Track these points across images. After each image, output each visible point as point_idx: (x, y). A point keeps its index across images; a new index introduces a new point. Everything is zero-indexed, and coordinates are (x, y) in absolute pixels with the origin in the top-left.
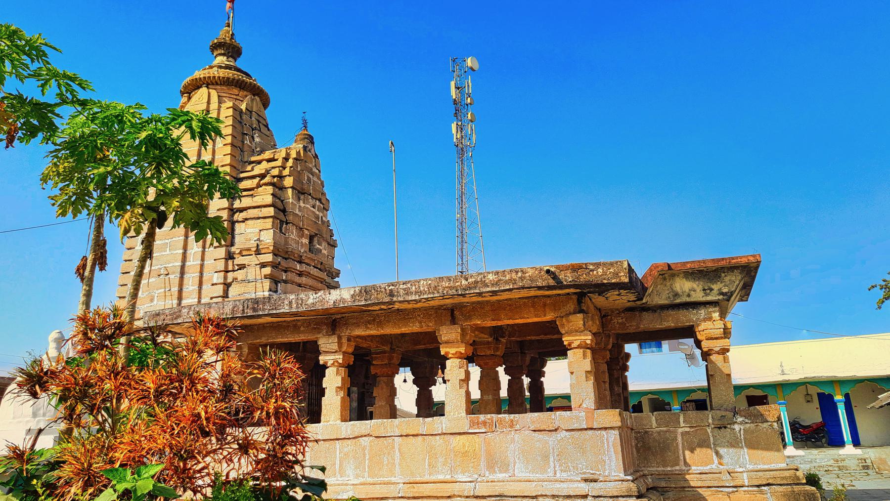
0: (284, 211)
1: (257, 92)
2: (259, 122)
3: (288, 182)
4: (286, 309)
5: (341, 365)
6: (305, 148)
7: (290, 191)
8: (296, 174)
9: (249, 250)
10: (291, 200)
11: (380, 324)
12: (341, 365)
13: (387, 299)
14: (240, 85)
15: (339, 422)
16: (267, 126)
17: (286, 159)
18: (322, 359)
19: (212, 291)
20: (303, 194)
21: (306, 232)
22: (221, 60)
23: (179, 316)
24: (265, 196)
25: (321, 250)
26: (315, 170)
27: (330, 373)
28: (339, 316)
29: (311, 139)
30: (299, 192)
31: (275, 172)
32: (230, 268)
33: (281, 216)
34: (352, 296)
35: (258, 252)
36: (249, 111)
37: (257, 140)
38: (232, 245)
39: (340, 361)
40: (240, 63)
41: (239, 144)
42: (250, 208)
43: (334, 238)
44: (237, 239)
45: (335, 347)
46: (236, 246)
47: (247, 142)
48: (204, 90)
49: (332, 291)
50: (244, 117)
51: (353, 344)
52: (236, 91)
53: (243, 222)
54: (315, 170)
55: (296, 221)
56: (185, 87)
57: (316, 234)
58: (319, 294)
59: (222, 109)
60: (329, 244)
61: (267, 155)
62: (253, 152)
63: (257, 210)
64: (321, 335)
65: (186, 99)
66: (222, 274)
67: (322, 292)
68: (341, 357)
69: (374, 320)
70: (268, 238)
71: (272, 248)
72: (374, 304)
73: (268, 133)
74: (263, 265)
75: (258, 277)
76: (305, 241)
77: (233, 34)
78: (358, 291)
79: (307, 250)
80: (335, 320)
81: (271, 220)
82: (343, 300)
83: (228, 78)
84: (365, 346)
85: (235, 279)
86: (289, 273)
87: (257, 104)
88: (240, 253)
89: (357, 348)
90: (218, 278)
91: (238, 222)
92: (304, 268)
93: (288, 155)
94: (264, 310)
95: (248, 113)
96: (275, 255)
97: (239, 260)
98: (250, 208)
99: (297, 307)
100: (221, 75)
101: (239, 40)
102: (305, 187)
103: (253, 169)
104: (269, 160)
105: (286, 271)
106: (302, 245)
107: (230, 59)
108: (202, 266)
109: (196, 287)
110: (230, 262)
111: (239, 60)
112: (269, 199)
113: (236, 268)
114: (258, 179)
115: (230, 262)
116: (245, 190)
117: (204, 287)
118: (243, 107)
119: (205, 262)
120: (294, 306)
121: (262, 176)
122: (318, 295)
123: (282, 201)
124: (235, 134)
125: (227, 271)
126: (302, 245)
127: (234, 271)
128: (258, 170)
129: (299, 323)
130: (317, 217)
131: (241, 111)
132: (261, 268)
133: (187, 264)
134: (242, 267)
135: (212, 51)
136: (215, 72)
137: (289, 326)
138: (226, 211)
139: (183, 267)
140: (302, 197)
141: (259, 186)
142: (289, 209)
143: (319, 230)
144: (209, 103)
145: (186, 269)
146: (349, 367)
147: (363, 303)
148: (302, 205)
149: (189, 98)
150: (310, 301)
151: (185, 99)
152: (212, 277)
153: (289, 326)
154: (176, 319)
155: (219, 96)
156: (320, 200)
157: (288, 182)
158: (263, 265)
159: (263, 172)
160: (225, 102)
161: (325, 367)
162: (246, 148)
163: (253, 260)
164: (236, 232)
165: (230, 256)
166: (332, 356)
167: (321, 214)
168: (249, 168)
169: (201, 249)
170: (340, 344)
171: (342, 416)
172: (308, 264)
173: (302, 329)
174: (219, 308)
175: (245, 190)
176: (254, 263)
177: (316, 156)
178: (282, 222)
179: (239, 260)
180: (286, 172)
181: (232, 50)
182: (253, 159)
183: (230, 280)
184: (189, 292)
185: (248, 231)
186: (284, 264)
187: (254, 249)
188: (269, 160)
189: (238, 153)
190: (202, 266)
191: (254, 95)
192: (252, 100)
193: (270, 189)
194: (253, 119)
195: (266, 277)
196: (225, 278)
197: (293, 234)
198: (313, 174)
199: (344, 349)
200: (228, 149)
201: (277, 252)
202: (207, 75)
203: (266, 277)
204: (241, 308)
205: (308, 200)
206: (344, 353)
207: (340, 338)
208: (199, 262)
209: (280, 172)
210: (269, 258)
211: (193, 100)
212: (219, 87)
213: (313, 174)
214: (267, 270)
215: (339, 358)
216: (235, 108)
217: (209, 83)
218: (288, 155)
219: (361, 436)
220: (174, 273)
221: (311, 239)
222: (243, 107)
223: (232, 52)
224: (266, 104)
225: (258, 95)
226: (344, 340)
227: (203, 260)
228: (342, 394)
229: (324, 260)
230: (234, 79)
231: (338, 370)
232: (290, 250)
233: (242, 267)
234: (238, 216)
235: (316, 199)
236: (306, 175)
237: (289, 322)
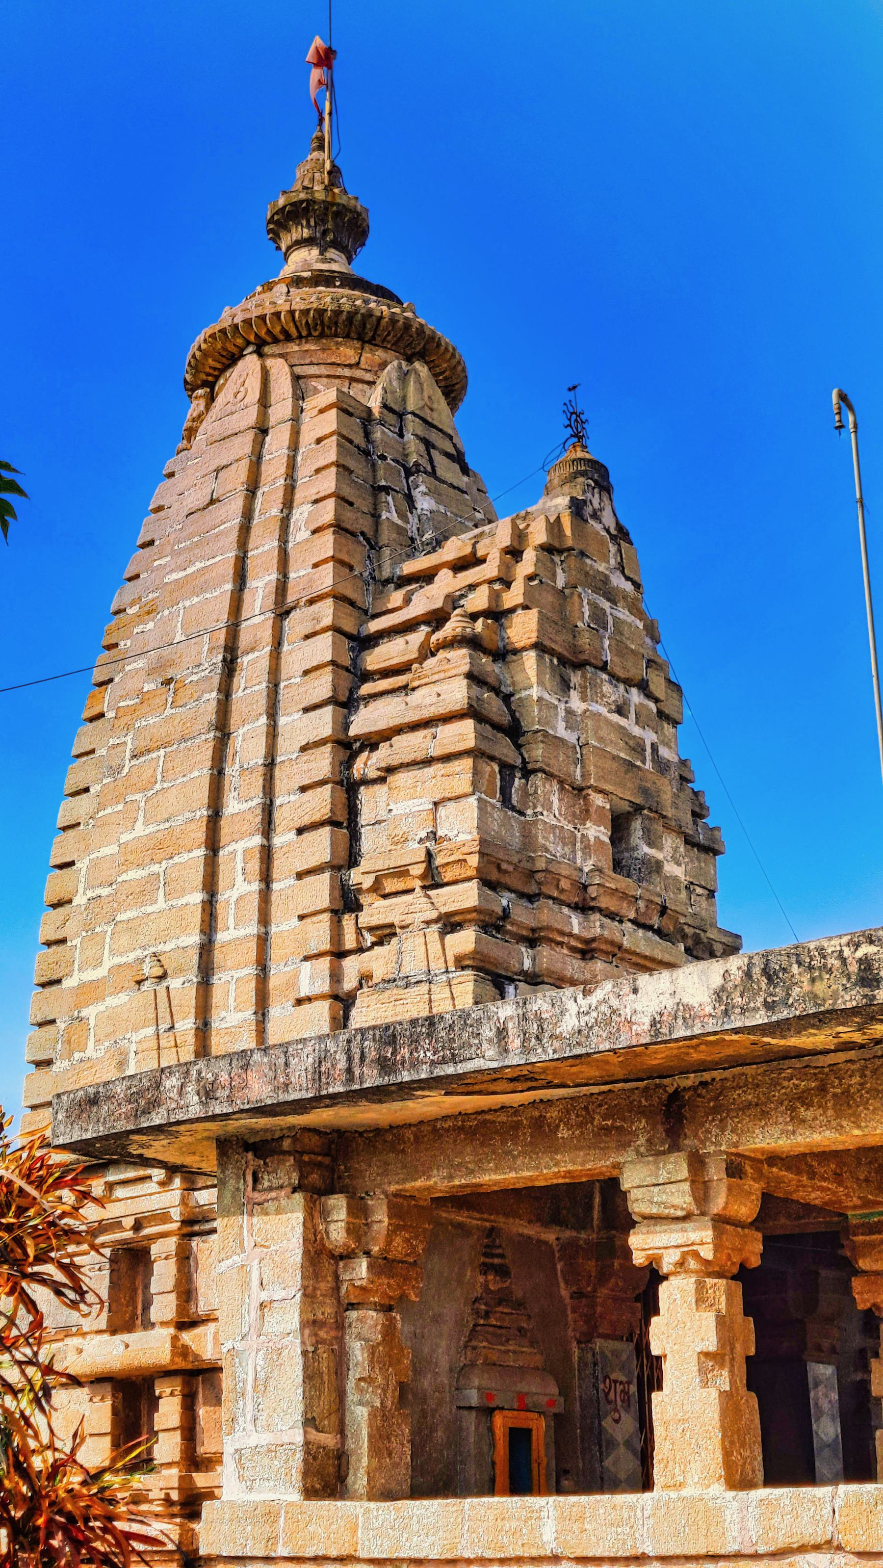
0: (514, 731)
1: (414, 345)
2: (428, 445)
3: (523, 629)
4: (487, 1059)
5: (710, 1269)
6: (577, 507)
7: (530, 659)
8: (549, 598)
9: (401, 872)
10: (535, 692)
11: (846, 1104)
12: (710, 1269)
13: (851, 999)
14: (361, 330)
15: (718, 1489)
16: (458, 458)
17: (514, 553)
18: (641, 1244)
19: (301, 1023)
20: (579, 666)
21: (598, 800)
22: (305, 259)
23: (155, 1103)
24: (446, 684)
25: (657, 866)
26: (618, 581)
27: (674, 1294)
28: (691, 1080)
29: (599, 476)
30: (563, 661)
31: (479, 600)
32: (350, 942)
33: (505, 749)
34: (719, 994)
35: (432, 880)
36: (396, 413)
37: (424, 504)
38: (353, 859)
39: (707, 1253)
40: (364, 265)
41: (365, 524)
42: (399, 730)
43: (710, 821)
44: (368, 841)
45: (681, 1197)
46: (365, 864)
47: (390, 514)
48: (250, 364)
49: (643, 980)
50: (378, 434)
51: (756, 1187)
52: (348, 352)
53: (382, 780)
54: (618, 581)
55: (559, 763)
56: (196, 366)
57: (638, 809)
58: (599, 994)
59: (306, 417)
60: (690, 842)
61: (453, 549)
62: (411, 548)
63: (421, 734)
64: (629, 1155)
65: (202, 403)
66: (325, 963)
67: (608, 986)
68: (708, 1235)
69: (822, 1089)
70: (461, 826)
71: (474, 861)
72: (803, 1022)
73: (463, 481)
74: (450, 924)
75: (437, 966)
76: (597, 832)
77: (335, 172)
78: (737, 975)
79: (606, 864)
80: (676, 1095)
81: (467, 763)
82: (685, 1012)
83: (321, 312)
84: (815, 1197)
85: (365, 978)
86: (544, 951)
87: (421, 389)
88: (376, 888)
89: (770, 1203)
90: (312, 982)
91: (366, 782)
92: (596, 927)
93: (520, 536)
94: (415, 1064)
95: (391, 418)
96: (488, 884)
97: (375, 912)
98: (399, 730)
99: (525, 1049)
100: (298, 305)
101: (357, 192)
102: (585, 640)
103: (407, 601)
104: (460, 566)
105: (532, 942)
106: (587, 848)
107: (332, 253)
108: (263, 941)
109: (249, 1014)
110: (348, 921)
111: (364, 255)
112: (457, 694)
113: (369, 939)
114: (424, 629)
115: (348, 921)
116: (386, 673)
117: (275, 1012)
118: (374, 402)
119: (274, 929)
120: (515, 1043)
121: (437, 619)
122: (593, 999)
123: (507, 699)
124: (347, 492)
125: (339, 954)
126: (587, 848)
127: (360, 950)
128: (426, 599)
129: (553, 1114)
130: (638, 748)
131: (367, 419)
132: (443, 933)
133: (221, 937)
134: (385, 934)
135: (276, 239)
136: (280, 299)
137: (516, 1126)
138: (328, 748)
139: (206, 949)
140: (576, 678)
141: (427, 652)
142: (532, 719)
143: (645, 791)
144: (264, 402)
145: (218, 956)
146: (743, 1275)
147: (760, 1018)
148: (577, 704)
149: (211, 399)
150: (569, 1024)
151: (197, 406)
152: (296, 975)
153: (517, 1126)
154: (146, 1112)
155: (297, 379)
156: (643, 686)
157: (523, 629)
158: (450, 924)
159: (439, 604)
160: (316, 391)
161: (654, 1276)
162: (386, 535)
163: (415, 908)
164: (363, 819)
165: (347, 902)
166: (677, 1227)
167: (649, 737)
168: (396, 597)
169: (256, 886)
170: (701, 1190)
171: (728, 1464)
172: (612, 916)
173: (563, 1133)
174: (274, 1067)
175: (386, 673)
176: (419, 918)
177: (621, 535)
178: (507, 769)
179: (375, 912)
180: (514, 596)
181: (341, 227)
182: (409, 567)
183: (349, 983)
184: (228, 1031)
185: (399, 809)
186: (524, 916)
187: (418, 870)
188: (460, 566)
189: (357, 554)
190: (263, 941)
191: (409, 360)
192: (404, 377)
193: (460, 659)
194: (409, 437)
195: (461, 963)
196: (336, 976)
197: (551, 808)
198: (612, 596)
199: (718, 1203)
200: (326, 544)
201: (494, 876)
202: (255, 313)
203: (461, 963)
204: (342, 1064)
205: (595, 685)
206: (721, 1222)
207: (697, 1163)
208: (253, 929)
209: (495, 597)
210: (465, 896)
211: (220, 400)
212: (294, 347)
213: (612, 596)
214: (465, 940)
215: (701, 1236)
216: (345, 408)
217: (264, 337)
218: (520, 536)
219: (803, 1549)
220: (180, 970)
221: (619, 825)
222: (374, 402)
223: (337, 229)
224: (453, 390)
225: (422, 356)
226: (716, 1172)
227: (264, 919)
228: (723, 1380)
229: (677, 900)
230: (338, 313)
231: (700, 1287)
232: (541, 864)
233: (385, 934)
234: (366, 765)
235: (628, 683)
236: (584, 604)
237: (516, 1111)
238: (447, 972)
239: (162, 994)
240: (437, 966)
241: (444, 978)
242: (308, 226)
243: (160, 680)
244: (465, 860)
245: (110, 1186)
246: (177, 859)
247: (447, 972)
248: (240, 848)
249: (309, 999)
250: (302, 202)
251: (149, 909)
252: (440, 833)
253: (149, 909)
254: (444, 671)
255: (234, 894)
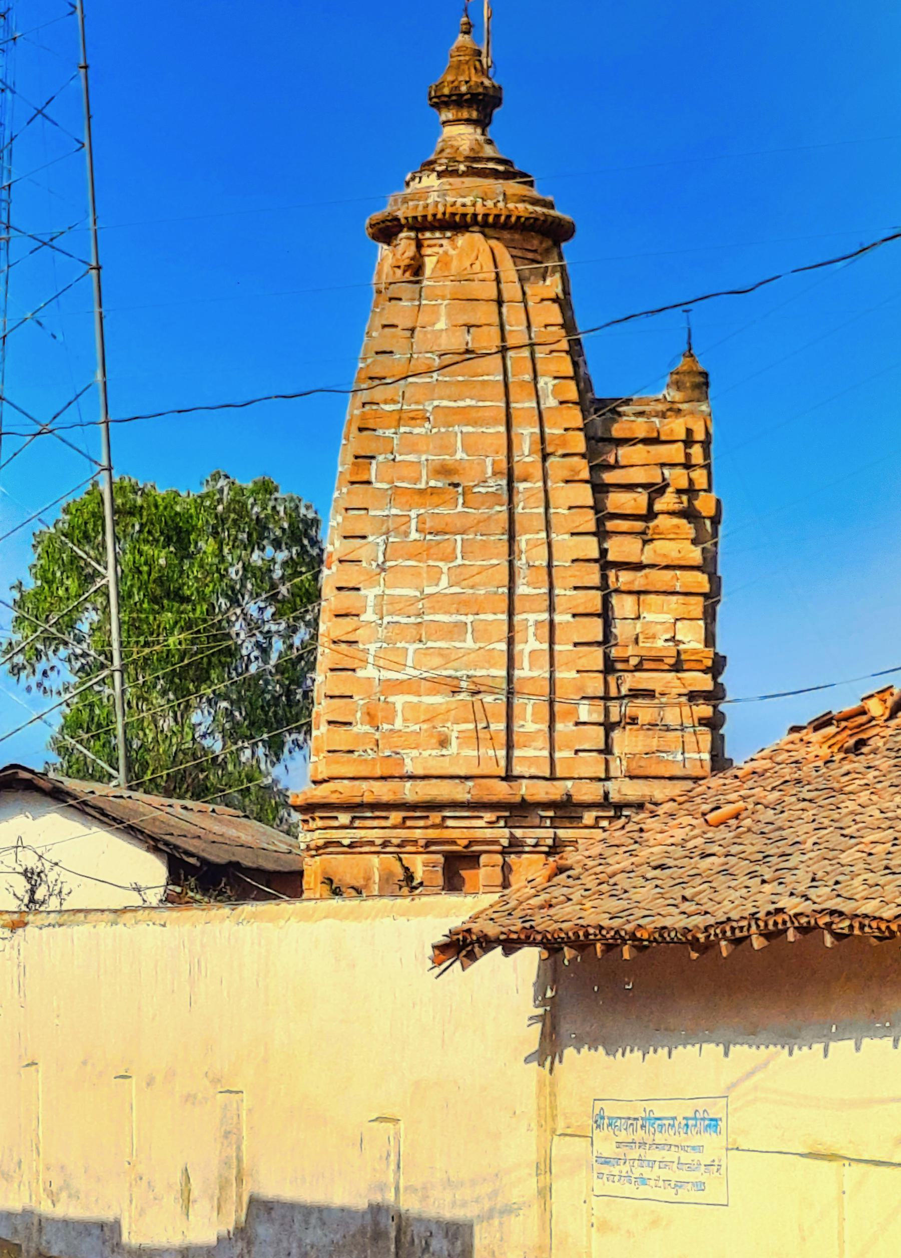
176: (676, 691)
181: (482, 105)
238: (694, 726)
239: (478, 705)
240: (687, 722)
241: (691, 730)
242: (477, 110)
243: (449, 482)
244: (701, 661)
245: (444, 818)
246: (482, 617)
247: (694, 726)
248: (531, 619)
249: (585, 723)
250: (479, 94)
251: (458, 644)
252: (678, 638)
253: (458, 644)
254: (677, 534)
255: (528, 648)
